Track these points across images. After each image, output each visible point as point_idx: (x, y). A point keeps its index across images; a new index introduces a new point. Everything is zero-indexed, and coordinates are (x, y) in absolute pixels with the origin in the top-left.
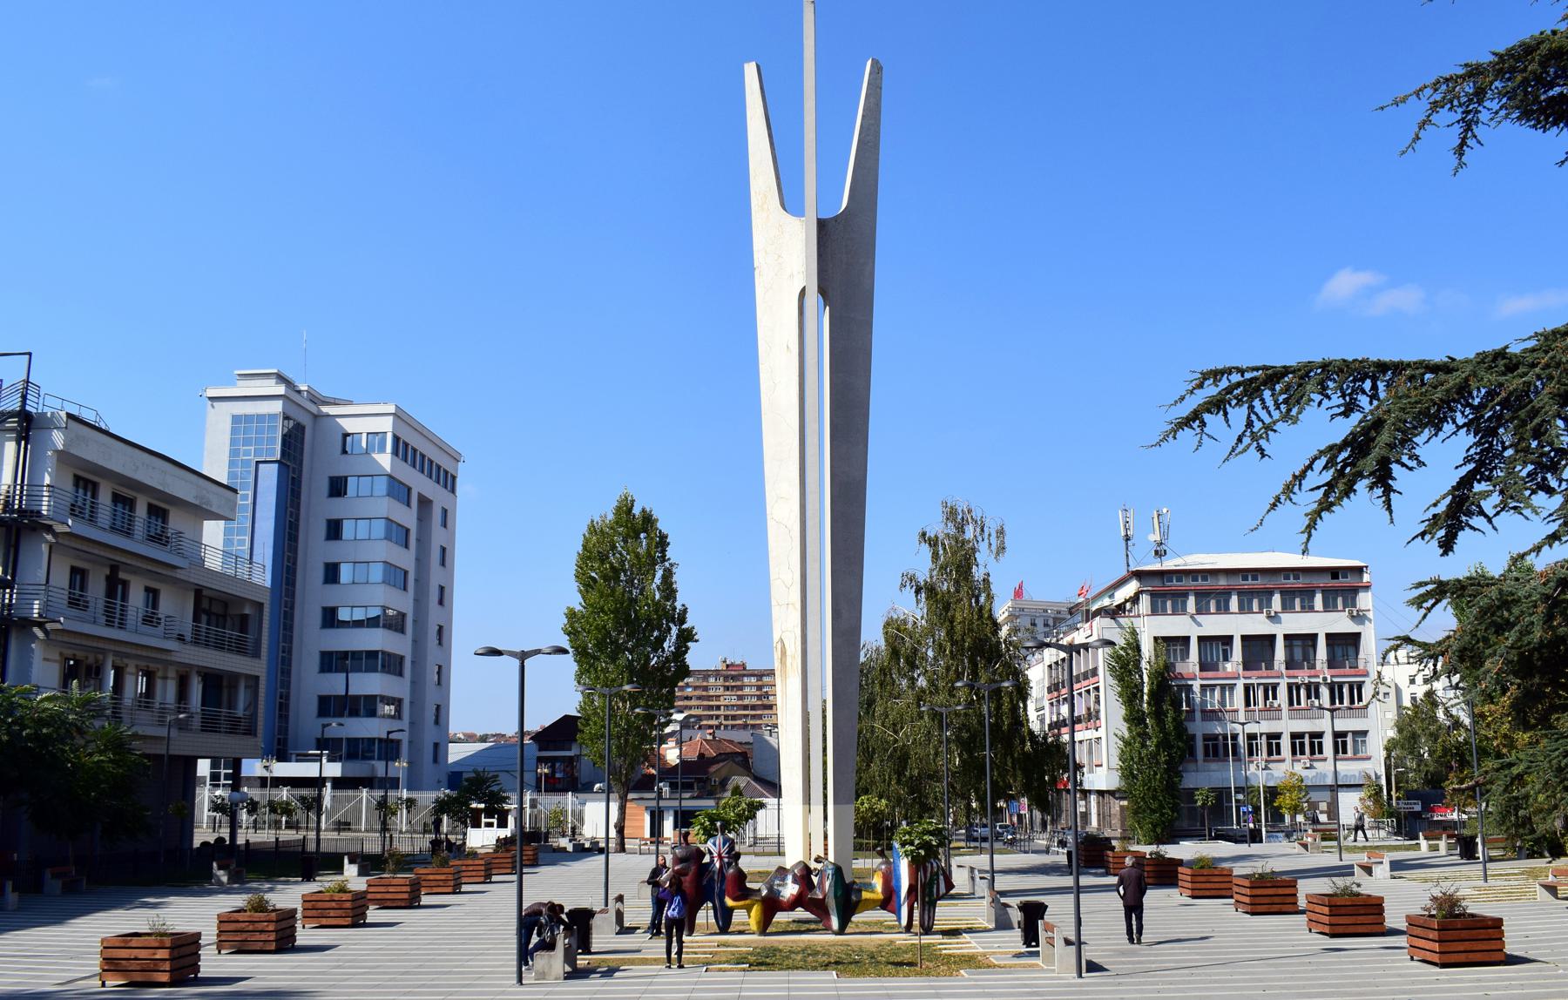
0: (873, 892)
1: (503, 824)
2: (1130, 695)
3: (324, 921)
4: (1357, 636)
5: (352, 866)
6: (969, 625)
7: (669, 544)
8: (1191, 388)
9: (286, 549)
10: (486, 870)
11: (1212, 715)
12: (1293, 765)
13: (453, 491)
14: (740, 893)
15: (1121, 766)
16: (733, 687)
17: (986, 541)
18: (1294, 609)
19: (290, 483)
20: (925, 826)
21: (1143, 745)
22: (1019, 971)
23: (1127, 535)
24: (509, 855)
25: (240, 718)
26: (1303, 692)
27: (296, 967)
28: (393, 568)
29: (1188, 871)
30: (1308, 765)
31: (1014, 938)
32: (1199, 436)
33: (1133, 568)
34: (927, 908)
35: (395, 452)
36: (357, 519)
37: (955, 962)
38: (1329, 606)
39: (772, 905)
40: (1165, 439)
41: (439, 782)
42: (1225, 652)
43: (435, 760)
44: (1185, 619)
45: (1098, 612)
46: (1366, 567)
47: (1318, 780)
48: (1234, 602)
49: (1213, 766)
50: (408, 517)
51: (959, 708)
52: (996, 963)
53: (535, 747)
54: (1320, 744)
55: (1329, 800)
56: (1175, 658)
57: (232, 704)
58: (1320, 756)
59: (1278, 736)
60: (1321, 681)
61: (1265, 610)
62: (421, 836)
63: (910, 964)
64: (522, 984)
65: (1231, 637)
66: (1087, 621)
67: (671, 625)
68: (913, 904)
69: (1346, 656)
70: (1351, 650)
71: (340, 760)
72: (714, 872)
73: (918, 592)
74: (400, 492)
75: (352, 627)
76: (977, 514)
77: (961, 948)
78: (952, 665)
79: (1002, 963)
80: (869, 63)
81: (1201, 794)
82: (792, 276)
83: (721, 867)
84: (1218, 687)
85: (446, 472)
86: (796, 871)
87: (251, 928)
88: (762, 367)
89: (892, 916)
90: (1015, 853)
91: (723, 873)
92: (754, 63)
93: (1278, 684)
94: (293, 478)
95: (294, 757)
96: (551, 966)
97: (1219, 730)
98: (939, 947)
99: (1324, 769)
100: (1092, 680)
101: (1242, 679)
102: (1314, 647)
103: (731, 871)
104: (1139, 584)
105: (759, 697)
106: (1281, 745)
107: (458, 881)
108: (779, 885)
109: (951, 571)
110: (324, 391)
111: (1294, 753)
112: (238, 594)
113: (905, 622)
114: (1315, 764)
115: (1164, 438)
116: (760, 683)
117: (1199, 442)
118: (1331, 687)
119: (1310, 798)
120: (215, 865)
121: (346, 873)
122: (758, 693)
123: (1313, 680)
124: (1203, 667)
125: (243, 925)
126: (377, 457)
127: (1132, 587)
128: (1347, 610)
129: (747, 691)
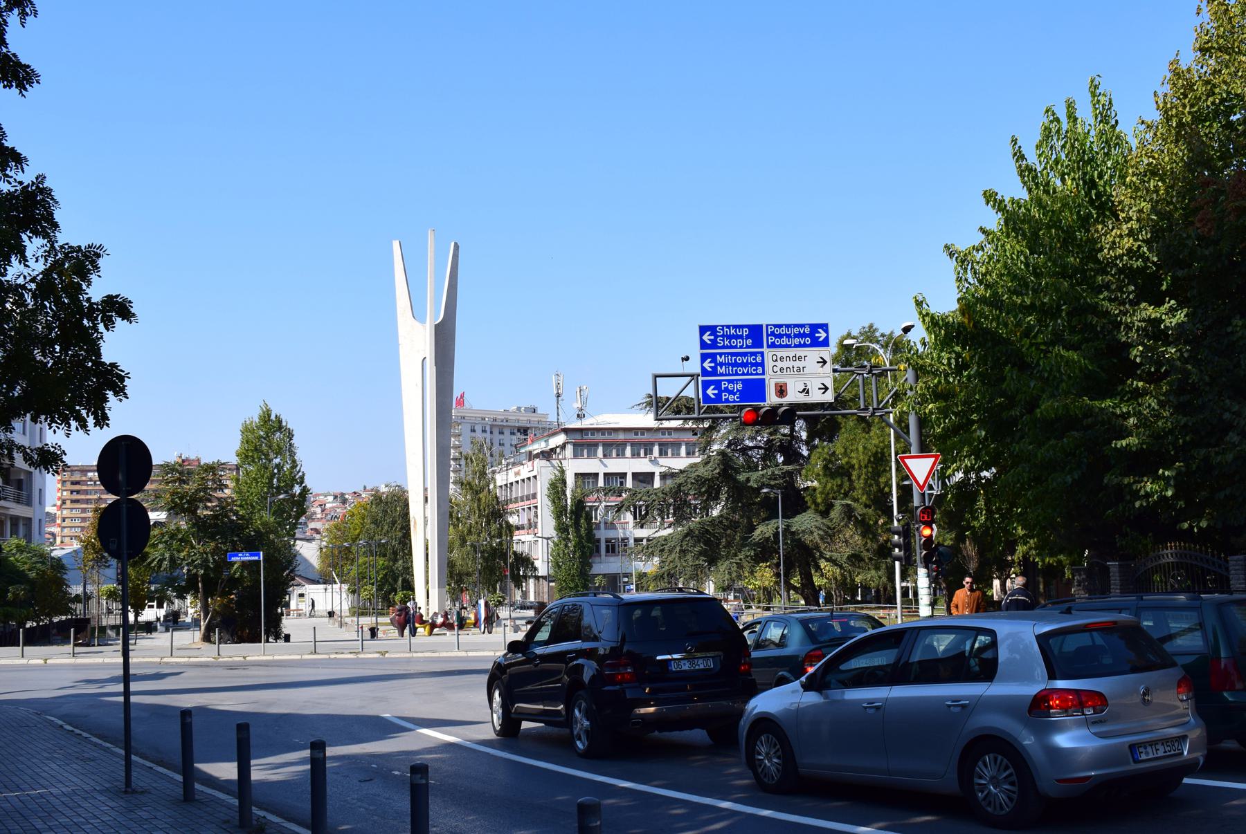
2: (559, 512)
21: (566, 546)
39: (433, 625)
48: (628, 451)
49: (612, 559)
65: (626, 474)
100: (535, 501)
127: (560, 439)
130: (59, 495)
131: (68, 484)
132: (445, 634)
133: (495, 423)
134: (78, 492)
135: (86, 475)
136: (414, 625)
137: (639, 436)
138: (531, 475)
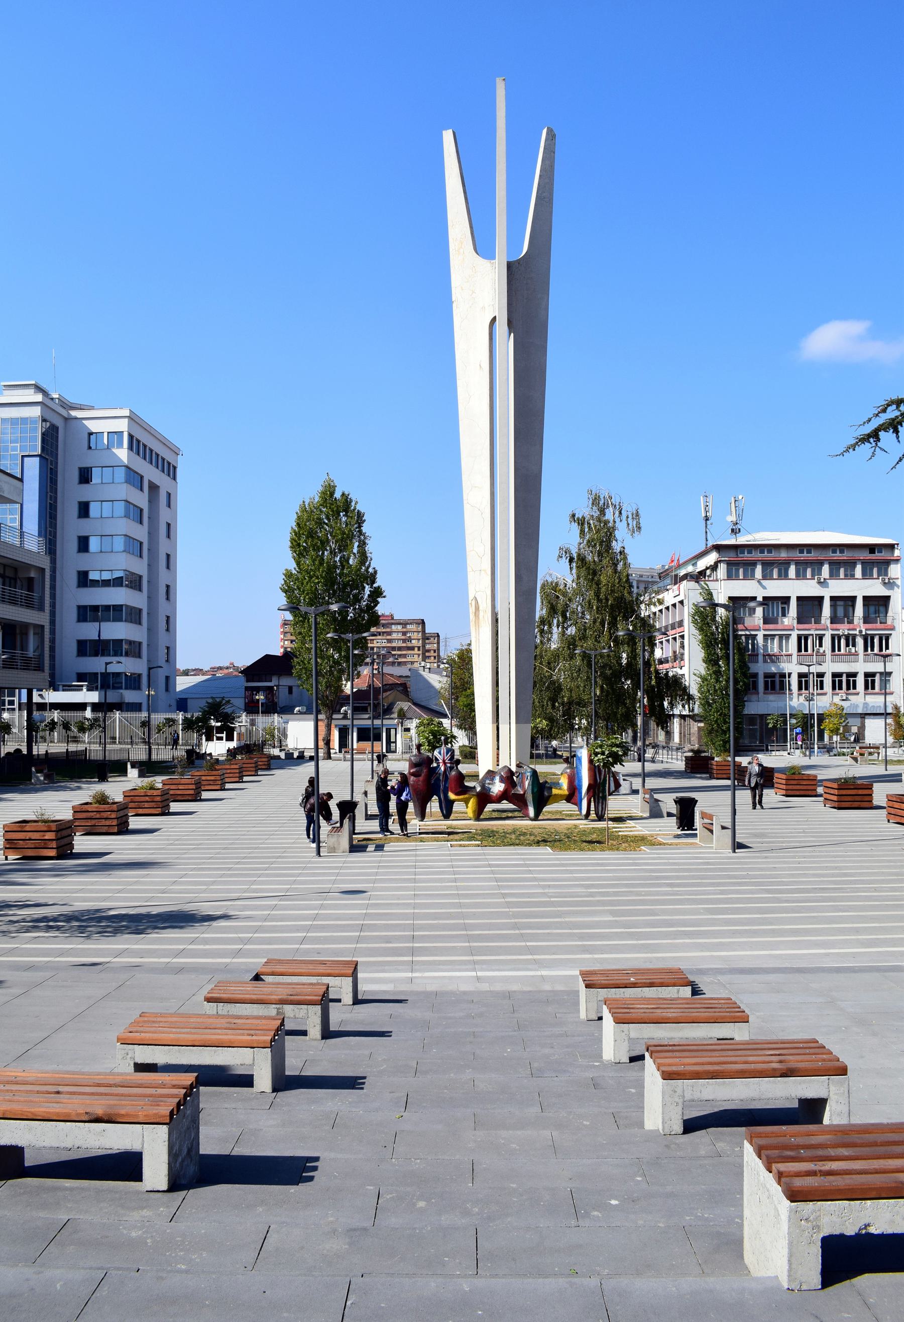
0: (560, 789)
1: (230, 738)
2: (709, 643)
3: (140, 811)
4: (888, 598)
5: (134, 769)
6: (611, 587)
7: (364, 521)
8: (877, 412)
9: (48, 526)
11: (772, 658)
12: (865, 697)
13: (174, 478)
15: (700, 697)
16: (384, 633)
18: (873, 576)
19: (49, 473)
20: (614, 741)
21: (717, 681)
23: (706, 516)
24: (253, 761)
25: (31, 658)
26: (843, 642)
27: (140, 844)
28: (131, 540)
29: (784, 777)
30: (844, 698)
31: (670, 825)
32: (874, 448)
33: (711, 543)
34: (600, 801)
35: (131, 448)
36: (102, 501)
38: (866, 575)
39: (484, 798)
40: (847, 451)
41: (170, 706)
42: (783, 609)
43: (167, 690)
46: (898, 544)
47: (852, 710)
49: (771, 697)
50: (141, 499)
51: (605, 651)
52: (664, 842)
54: (854, 682)
55: (859, 725)
56: (745, 614)
57: (24, 647)
58: (854, 691)
59: (855, 675)
60: (858, 633)
61: (816, 577)
62: (163, 747)
63: (599, 842)
64: (320, 856)
66: (675, 583)
68: (591, 799)
69: (877, 612)
70: (882, 609)
71: (97, 689)
72: (440, 774)
73: (571, 560)
74: (134, 478)
75: (102, 586)
77: (631, 831)
78: (598, 618)
79: (670, 842)
80: (545, 131)
81: (772, 719)
82: (483, 308)
83: (445, 770)
84: (777, 637)
85: (169, 464)
86: (502, 773)
87: (98, 816)
88: (459, 383)
89: (575, 807)
90: (630, 762)
91: (446, 775)
93: (824, 635)
94: (51, 469)
95: (61, 687)
97: (773, 669)
98: (614, 830)
99: (860, 700)
100: (678, 630)
102: (853, 606)
103: (453, 773)
105: (404, 641)
106: (825, 682)
107: (224, 781)
108: (489, 784)
109: (595, 545)
110: (71, 399)
111: (834, 688)
112: (26, 562)
113: (557, 584)
114: (850, 697)
115: (847, 450)
117: (873, 453)
118: (865, 638)
119: (848, 723)
120: (33, 769)
121: (129, 775)
122: (403, 637)
123: (851, 632)
124: (766, 621)
125: (92, 814)
126: (116, 451)
127: (712, 557)
128: (881, 578)
129: (394, 636)
130: (282, 644)
133: (641, 579)
136: (446, 796)
137: (805, 554)
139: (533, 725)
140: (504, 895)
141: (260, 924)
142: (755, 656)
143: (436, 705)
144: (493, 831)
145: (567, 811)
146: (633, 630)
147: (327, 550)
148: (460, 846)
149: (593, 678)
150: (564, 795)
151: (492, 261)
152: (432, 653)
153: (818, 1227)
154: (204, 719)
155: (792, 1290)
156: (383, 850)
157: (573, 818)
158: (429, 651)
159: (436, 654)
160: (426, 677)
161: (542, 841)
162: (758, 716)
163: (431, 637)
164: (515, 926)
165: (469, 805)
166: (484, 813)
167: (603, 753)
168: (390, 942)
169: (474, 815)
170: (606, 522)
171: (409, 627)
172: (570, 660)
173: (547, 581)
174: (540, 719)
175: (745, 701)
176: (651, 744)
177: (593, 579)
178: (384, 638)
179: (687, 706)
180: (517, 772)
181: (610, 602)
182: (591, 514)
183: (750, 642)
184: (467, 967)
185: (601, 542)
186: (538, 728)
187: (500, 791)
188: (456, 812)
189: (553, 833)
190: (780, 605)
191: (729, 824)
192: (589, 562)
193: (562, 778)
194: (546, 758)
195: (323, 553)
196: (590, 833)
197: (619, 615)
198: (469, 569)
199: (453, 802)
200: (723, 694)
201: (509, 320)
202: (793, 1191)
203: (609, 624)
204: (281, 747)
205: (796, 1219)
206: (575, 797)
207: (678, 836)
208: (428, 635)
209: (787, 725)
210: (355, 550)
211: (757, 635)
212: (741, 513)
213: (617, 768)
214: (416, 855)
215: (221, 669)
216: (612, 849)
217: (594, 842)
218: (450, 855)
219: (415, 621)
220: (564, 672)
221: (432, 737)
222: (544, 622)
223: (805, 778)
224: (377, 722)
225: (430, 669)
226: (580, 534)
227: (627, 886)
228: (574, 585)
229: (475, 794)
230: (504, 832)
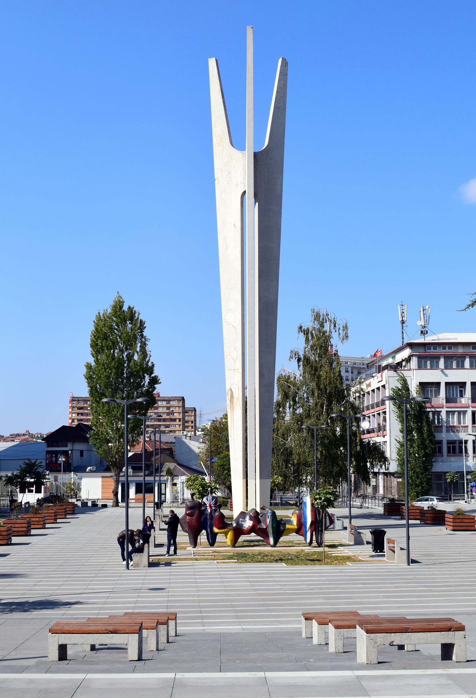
0: (292, 525)
7: (145, 327)
10: (55, 516)
11: (451, 429)
14: (222, 525)
15: (398, 459)
17: (337, 332)
20: (327, 490)
21: (411, 446)
22: (376, 563)
23: (403, 320)
29: (451, 516)
33: (406, 341)
37: (340, 559)
39: (239, 531)
42: (461, 391)
44: (438, 372)
45: (386, 367)
49: (453, 459)
51: (323, 426)
52: (363, 559)
53: (45, 445)
56: (432, 395)
64: (129, 569)
66: (379, 372)
67: (145, 375)
72: (207, 514)
73: (299, 360)
76: (331, 317)
77: (341, 553)
78: (319, 402)
79: (366, 559)
80: (280, 60)
82: (237, 184)
83: (211, 511)
84: (456, 415)
86: (251, 514)
88: (219, 236)
89: (301, 538)
90: (344, 508)
91: (212, 515)
92: (214, 59)
96: (141, 560)
98: (329, 552)
101: (471, 407)
103: (217, 514)
104: (411, 351)
105: (168, 414)
108: (242, 521)
109: (317, 349)
113: (289, 377)
115: (468, 307)
116: (168, 405)
122: (167, 411)
127: (406, 353)
130: (70, 416)
131: (76, 409)
132: (473, 461)
134: (82, 414)
135: (87, 404)
138: (380, 385)
139: (271, 480)
140: (255, 590)
141: (102, 606)
142: (439, 428)
143: (195, 465)
144: (245, 554)
145: (296, 541)
146: (344, 410)
147: (117, 349)
148: (223, 563)
149: (315, 446)
150: (294, 529)
151: (243, 152)
152: (190, 424)
153: (376, 642)
154: (23, 475)
155: (368, 664)
156: (171, 566)
157: (301, 545)
158: (187, 422)
159: (193, 425)
160: (188, 443)
161: (279, 560)
162: (443, 473)
163: (189, 410)
164: (263, 605)
165: (228, 536)
166: (238, 543)
167: (320, 499)
168: (187, 614)
169: (231, 544)
170: (324, 333)
171: (172, 403)
172: (299, 432)
173: (282, 374)
174: (276, 476)
175: (433, 462)
176: (361, 495)
177: (315, 374)
178: (152, 411)
179: (383, 466)
180: (261, 513)
181: (328, 391)
182: (314, 326)
183: (436, 417)
184: (236, 624)
185: (320, 347)
186: (275, 482)
187: (249, 526)
188: (218, 542)
189: (286, 555)
190: (458, 388)
191: (405, 546)
192: (312, 361)
193: (293, 517)
194: (281, 505)
195: (114, 352)
196: (312, 555)
197: (334, 400)
198: (226, 368)
199: (216, 534)
200: (416, 457)
201: (255, 193)
202: (367, 630)
203: (327, 406)
204: (76, 498)
205: (369, 639)
206: (302, 530)
207: (373, 556)
208: (187, 409)
209: (464, 481)
210: (138, 349)
211: (441, 411)
212: (428, 319)
213: (330, 510)
214: (194, 568)
215: (19, 436)
216: (327, 564)
217: (315, 560)
218: (217, 568)
219: (177, 398)
220: (294, 442)
221: (201, 489)
222: (280, 405)
223: (466, 517)
224: (148, 479)
225: (190, 437)
226: (306, 341)
227: (335, 584)
228: (301, 378)
229: (232, 528)
230: (253, 555)
